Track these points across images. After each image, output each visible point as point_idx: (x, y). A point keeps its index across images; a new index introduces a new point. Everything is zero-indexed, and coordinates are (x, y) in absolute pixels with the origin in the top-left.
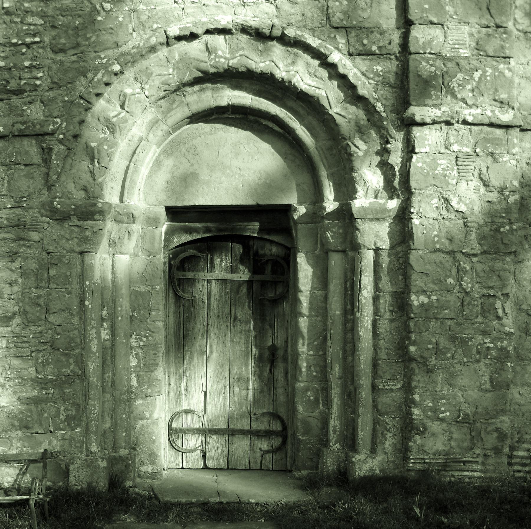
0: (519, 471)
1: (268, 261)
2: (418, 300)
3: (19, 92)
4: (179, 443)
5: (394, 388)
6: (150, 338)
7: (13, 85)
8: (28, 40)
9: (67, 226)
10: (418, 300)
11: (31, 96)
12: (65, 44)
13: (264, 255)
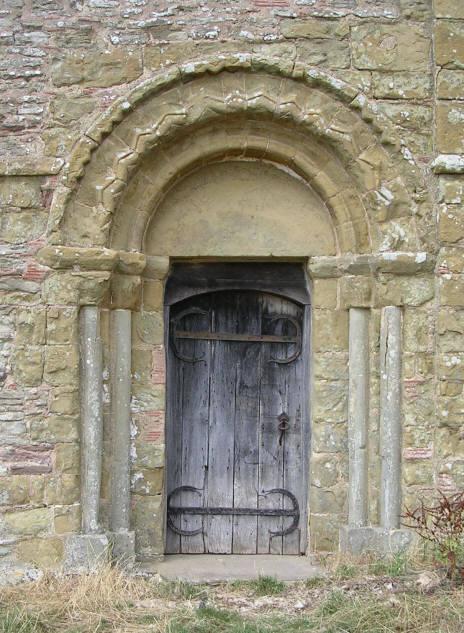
1: (278, 320)
3: (16, 129)
4: (176, 524)
5: (424, 456)
7: (10, 120)
8: (28, 73)
11: (29, 133)
12: (69, 78)
13: (275, 313)
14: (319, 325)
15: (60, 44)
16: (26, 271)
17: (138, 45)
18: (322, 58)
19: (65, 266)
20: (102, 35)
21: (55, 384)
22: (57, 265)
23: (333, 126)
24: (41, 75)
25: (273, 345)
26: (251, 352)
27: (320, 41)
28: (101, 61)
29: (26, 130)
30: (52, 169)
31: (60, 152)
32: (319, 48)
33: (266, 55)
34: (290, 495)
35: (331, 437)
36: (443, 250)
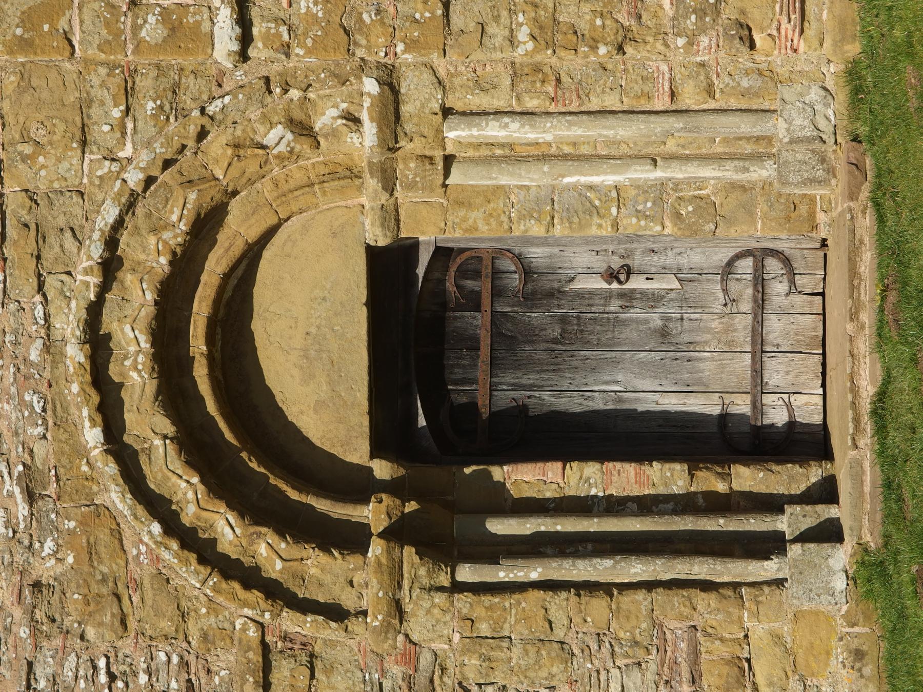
0: (663, 78)
2: (524, 43)
5: (667, 76)
6: (592, 481)
8: (103, 678)
9: (411, 606)
10: (524, 43)
12: (113, 615)
14: (471, 228)
15: (56, 630)
16: (403, 669)
17: (57, 513)
18: (68, 234)
19: (398, 610)
20: (46, 569)
21: (566, 622)
22: (396, 622)
23: (174, 218)
24: (107, 658)
25: (497, 293)
26: (507, 328)
27: (41, 236)
28: (86, 568)
29: (193, 677)
30: (253, 633)
31: (227, 625)
32: (52, 239)
33: (69, 324)
34: (730, 263)
35: (640, 207)
36: (360, 53)
